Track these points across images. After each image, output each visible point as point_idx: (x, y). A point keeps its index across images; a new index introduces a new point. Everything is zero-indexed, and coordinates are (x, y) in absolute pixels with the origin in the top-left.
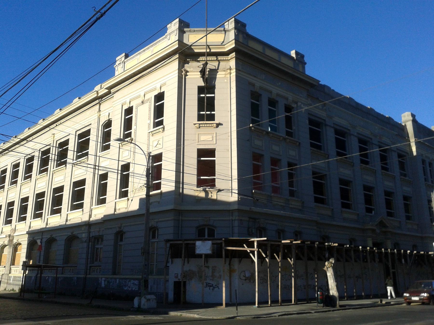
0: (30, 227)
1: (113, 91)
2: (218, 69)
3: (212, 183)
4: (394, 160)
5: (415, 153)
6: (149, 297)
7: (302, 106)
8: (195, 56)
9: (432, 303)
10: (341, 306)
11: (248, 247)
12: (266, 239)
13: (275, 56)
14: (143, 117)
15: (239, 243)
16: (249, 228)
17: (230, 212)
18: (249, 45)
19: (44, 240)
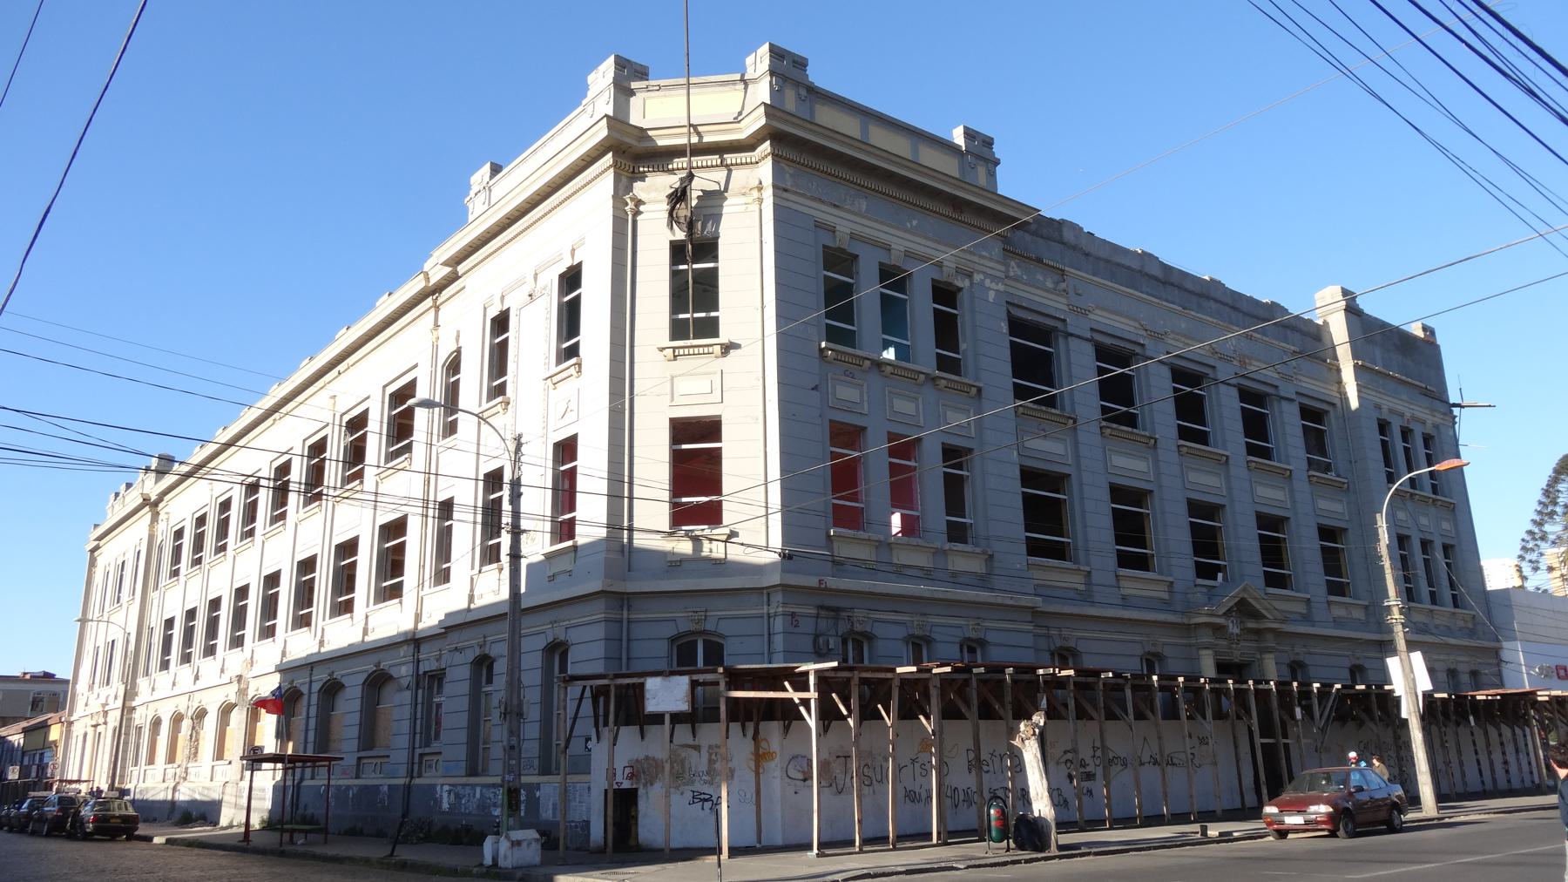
0: (284, 654)
1: (461, 269)
2: (726, 189)
3: (712, 515)
4: (1287, 427)
5: (1354, 403)
6: (517, 835)
7: (988, 282)
8: (661, 158)
9: (1341, 832)
10: (1061, 848)
11: (796, 689)
12: (835, 664)
13: (899, 145)
14: (534, 334)
15: (773, 679)
16: (817, 636)
17: (765, 592)
18: (818, 121)
19: (316, 687)
